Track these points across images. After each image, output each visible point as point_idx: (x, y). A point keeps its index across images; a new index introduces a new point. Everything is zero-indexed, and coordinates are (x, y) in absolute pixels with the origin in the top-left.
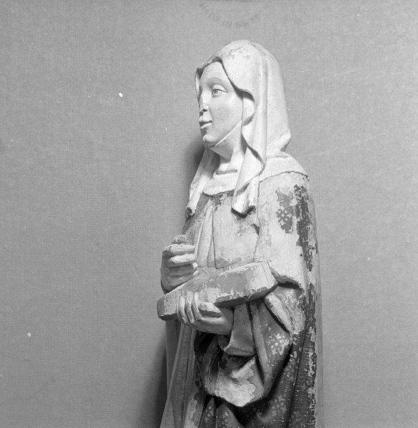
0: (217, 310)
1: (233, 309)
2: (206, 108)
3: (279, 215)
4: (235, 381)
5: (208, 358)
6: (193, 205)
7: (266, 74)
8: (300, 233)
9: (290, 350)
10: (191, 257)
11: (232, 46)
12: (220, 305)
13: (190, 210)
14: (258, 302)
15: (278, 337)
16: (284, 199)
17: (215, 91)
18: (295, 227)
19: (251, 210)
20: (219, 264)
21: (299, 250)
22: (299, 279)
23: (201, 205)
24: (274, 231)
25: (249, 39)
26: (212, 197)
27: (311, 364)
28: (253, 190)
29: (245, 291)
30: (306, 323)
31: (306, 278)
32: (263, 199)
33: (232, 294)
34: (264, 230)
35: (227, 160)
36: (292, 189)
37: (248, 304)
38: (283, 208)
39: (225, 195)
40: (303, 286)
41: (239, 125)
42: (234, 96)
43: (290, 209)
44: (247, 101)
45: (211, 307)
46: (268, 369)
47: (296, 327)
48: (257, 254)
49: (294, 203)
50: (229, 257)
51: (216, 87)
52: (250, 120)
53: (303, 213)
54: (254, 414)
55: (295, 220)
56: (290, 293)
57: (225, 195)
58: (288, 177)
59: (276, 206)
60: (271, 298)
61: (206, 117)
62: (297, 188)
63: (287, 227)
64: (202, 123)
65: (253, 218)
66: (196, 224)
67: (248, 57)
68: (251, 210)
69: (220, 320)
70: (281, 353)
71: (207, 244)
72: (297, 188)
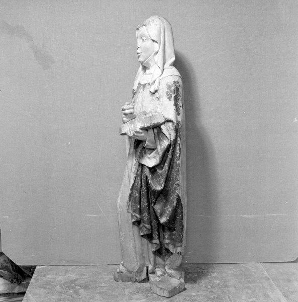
0: (140, 131)
1: (157, 264)
2: (139, 47)
3: (167, 93)
4: (149, 158)
5: (139, 149)
6: (135, 88)
7: (165, 32)
8: (175, 101)
9: (169, 146)
10: (132, 110)
11: (150, 19)
12: (142, 129)
13: (134, 90)
14: (157, 127)
15: (165, 141)
16: (169, 87)
17: (143, 39)
18: (173, 98)
19: (156, 91)
20: (145, 113)
21: (174, 107)
22: (174, 119)
23: (138, 88)
24: (165, 98)
25: (157, 14)
26: (142, 85)
27: (178, 151)
28: (157, 82)
29: (171, 54)
30: (176, 136)
31: (177, 118)
32: (161, 87)
33: (146, 125)
34: (161, 99)
35: (149, 69)
36: (173, 83)
37: (153, 129)
38: (168, 91)
39: (147, 85)
40: (175, 122)
41: (153, 54)
42: (151, 41)
43: (171, 91)
44: (155, 43)
45: (138, 130)
46: (161, 153)
47: (173, 138)
48: (158, 109)
49: (173, 88)
50: (148, 110)
51: (143, 38)
52: (157, 53)
53: (177, 92)
54: (156, 170)
55: (173, 96)
56: (171, 124)
57: (147, 85)
58: (171, 77)
59: (166, 90)
60: (162, 127)
61: (139, 51)
62: (175, 82)
63: (170, 98)
64: (138, 53)
65: (157, 94)
66: (136, 97)
67: (156, 25)
68: (156, 91)
69: (143, 134)
70: (166, 147)
71: (140, 105)
72: (175, 82)
